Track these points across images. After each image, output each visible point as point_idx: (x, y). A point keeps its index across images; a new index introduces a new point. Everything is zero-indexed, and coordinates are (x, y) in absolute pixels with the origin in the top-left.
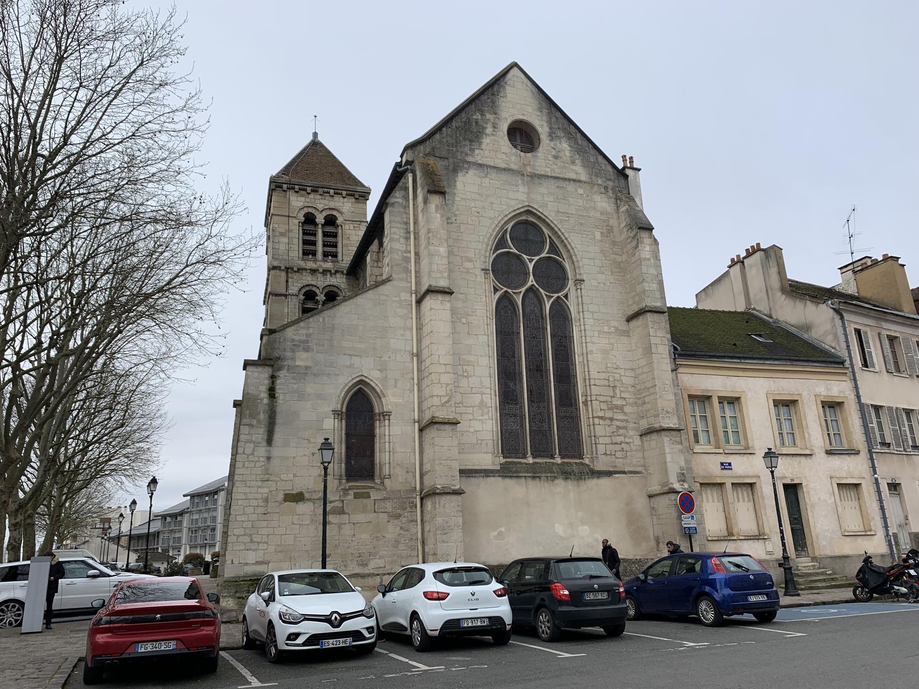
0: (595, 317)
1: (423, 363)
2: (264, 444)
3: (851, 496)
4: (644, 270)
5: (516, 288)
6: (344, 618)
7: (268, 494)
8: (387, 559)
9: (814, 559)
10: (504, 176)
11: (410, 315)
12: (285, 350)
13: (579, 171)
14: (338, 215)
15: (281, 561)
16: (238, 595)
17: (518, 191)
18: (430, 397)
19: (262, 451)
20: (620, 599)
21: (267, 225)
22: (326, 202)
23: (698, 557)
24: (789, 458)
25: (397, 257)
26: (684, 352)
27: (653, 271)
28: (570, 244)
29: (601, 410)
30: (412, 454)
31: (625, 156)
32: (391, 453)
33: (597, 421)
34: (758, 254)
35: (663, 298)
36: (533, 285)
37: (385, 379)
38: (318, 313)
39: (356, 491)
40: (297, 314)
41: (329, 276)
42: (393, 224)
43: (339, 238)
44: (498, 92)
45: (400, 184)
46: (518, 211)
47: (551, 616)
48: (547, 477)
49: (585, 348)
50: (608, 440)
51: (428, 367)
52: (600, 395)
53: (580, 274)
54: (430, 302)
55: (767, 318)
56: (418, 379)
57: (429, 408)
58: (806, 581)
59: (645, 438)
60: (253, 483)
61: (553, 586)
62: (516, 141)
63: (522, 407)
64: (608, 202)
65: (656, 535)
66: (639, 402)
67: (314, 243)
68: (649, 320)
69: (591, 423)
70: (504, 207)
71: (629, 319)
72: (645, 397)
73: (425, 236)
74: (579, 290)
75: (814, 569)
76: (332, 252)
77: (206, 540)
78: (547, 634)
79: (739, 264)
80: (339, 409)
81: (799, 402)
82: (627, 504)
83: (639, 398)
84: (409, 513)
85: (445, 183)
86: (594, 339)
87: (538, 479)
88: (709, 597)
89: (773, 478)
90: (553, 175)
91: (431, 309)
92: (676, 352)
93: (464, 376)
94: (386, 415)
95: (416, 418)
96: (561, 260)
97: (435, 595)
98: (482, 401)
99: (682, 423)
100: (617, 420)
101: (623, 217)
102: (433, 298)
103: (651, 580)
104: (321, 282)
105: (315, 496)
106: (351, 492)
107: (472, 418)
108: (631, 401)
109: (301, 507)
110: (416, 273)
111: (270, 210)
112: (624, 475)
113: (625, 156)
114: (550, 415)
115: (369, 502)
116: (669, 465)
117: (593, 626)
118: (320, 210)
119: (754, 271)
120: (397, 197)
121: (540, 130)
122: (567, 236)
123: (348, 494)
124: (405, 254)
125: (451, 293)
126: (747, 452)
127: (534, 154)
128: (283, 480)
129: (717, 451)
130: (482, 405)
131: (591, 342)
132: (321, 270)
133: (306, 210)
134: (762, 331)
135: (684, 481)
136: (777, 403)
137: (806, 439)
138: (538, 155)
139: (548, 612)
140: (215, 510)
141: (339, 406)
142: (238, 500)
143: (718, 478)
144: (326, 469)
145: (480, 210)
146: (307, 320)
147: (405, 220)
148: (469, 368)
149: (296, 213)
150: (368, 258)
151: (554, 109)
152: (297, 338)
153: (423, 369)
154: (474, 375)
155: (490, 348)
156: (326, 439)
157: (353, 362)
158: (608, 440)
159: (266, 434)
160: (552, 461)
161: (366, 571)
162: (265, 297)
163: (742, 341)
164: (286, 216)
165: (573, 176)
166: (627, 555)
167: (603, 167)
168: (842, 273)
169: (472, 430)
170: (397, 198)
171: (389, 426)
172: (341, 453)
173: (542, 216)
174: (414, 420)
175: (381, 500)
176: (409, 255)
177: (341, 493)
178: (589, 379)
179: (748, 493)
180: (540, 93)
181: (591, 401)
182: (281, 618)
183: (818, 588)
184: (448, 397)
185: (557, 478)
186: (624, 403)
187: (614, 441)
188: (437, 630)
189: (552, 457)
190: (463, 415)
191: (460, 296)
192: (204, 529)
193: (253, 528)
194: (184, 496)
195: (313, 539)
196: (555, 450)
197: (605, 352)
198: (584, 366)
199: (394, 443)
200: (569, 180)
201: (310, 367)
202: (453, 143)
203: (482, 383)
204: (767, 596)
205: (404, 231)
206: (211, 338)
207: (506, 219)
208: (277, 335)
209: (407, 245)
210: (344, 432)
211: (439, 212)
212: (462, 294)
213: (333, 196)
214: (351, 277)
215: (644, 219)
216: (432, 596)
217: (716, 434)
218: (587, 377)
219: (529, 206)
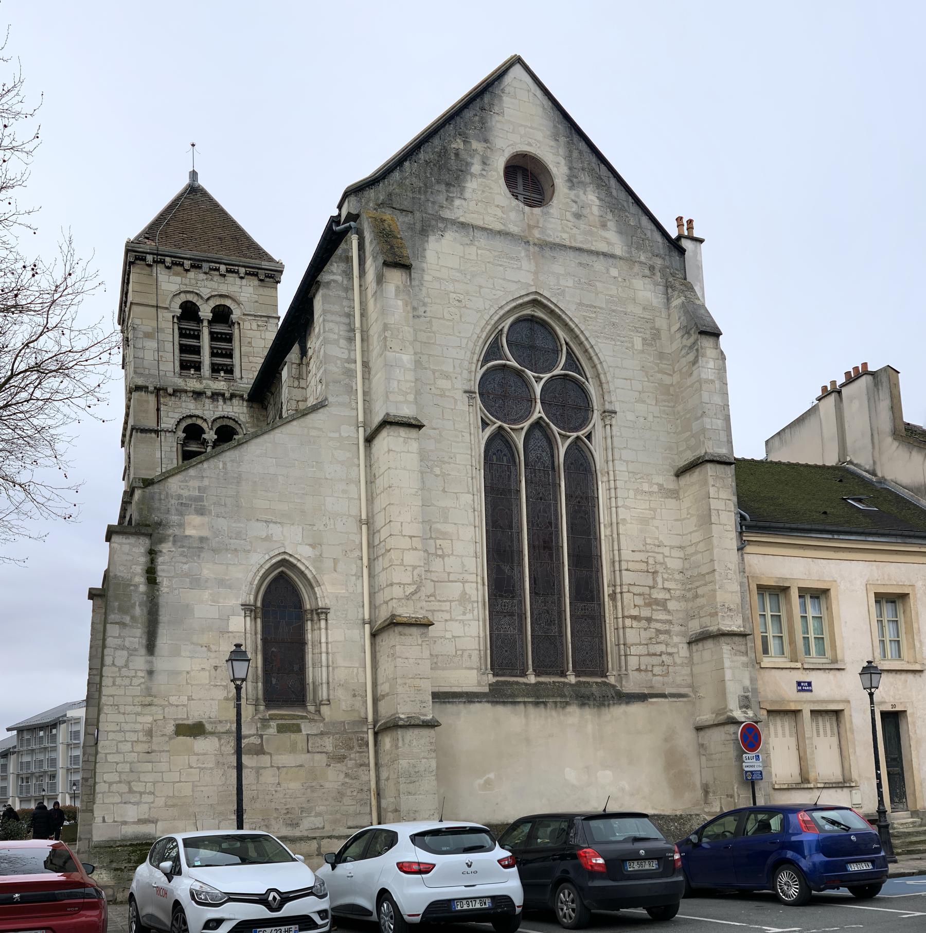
1: (377, 535)
2: (143, 651)
4: (705, 396)
5: (515, 422)
6: (286, 898)
7: (151, 724)
8: (327, 817)
9: (915, 813)
10: (499, 244)
11: (356, 460)
16: (114, 865)
17: (520, 268)
18: (387, 586)
19: (140, 662)
20: (674, 869)
21: (122, 320)
22: (214, 285)
23: (772, 811)
25: (335, 369)
26: (754, 523)
27: (717, 399)
28: (597, 355)
29: (635, 606)
30: (361, 670)
31: (681, 218)
32: (331, 668)
33: (628, 622)
34: (864, 380)
35: (730, 442)
36: (541, 418)
37: (319, 558)
38: (207, 459)
39: (280, 722)
40: (175, 461)
41: (221, 402)
42: (329, 317)
43: (236, 343)
44: (491, 105)
45: (339, 251)
46: (520, 301)
47: (578, 893)
48: (555, 703)
49: (614, 516)
50: (642, 650)
51: (384, 541)
52: (634, 585)
53: (611, 402)
54: (387, 440)
55: (868, 476)
56: (369, 559)
57: (386, 603)
58: (903, 842)
59: (694, 647)
60: (129, 709)
61: (581, 852)
62: (516, 188)
63: (522, 602)
64: (654, 292)
65: (704, 782)
66: (689, 595)
67: (197, 351)
68: (709, 474)
69: (621, 625)
71: (681, 472)
72: (697, 587)
73: (379, 336)
74: (608, 427)
75: (914, 826)
76: (225, 365)
77: (44, 790)
78: (571, 918)
79: (833, 394)
80: (252, 602)
81: (911, 596)
82: (666, 740)
83: (690, 590)
84: (357, 754)
85: (408, 252)
86: (629, 502)
87: (542, 706)
88: (792, 865)
89: (872, 702)
90: (574, 244)
91: (389, 451)
92: (744, 522)
93: (437, 555)
94: (321, 613)
95: (367, 617)
96: (583, 380)
97: (415, 867)
98: (464, 593)
99: (747, 626)
100: (657, 621)
101: (675, 315)
102: (392, 433)
103: (707, 843)
104: (210, 411)
105: (221, 728)
106: (273, 724)
107: (448, 618)
108: (678, 593)
109: (202, 744)
111: (126, 297)
112: (663, 700)
113: (681, 218)
114: (561, 614)
115: (299, 738)
117: (636, 907)
118: (206, 297)
119: (856, 405)
120: (333, 273)
121: (554, 169)
122: (593, 343)
123: (269, 727)
124: (346, 365)
125: (420, 427)
126: (835, 668)
128: (172, 705)
129: (793, 665)
130: (464, 598)
131: (624, 506)
132: (209, 393)
133: (183, 298)
134: (862, 494)
135: (747, 707)
136: (880, 598)
137: (917, 649)
138: (551, 211)
139: (573, 889)
140: (54, 749)
141: (252, 598)
142: (108, 732)
144: (238, 688)
145: (462, 297)
146: (200, 466)
147: (347, 310)
148: (445, 544)
149: (168, 302)
150: (285, 373)
151: (576, 138)
152: (185, 493)
153: (376, 544)
154: (452, 554)
155: (476, 513)
156: (238, 646)
157: (270, 532)
158: (642, 650)
160: (562, 680)
161: (297, 833)
162: (124, 435)
163: (834, 508)
164: (153, 306)
165: (602, 247)
166: (663, 810)
167: (649, 234)
169: (448, 635)
170: (334, 274)
171: (327, 629)
172: (257, 667)
173: (557, 310)
174: (364, 620)
176: (352, 366)
177: (259, 725)
178: (620, 561)
179: (831, 725)
180: (555, 109)
181: (621, 593)
182: (193, 898)
183: (919, 852)
184: (415, 587)
186: (668, 596)
187: (652, 651)
188: (419, 915)
189: (563, 674)
190: (435, 613)
191: (431, 432)
192: (40, 776)
193: (132, 772)
194: (9, 730)
195: (221, 789)
196: (568, 664)
197: (644, 521)
198: (613, 541)
199: (334, 654)
200: (598, 253)
202: (420, 188)
203: (463, 566)
204: (873, 865)
205: (343, 328)
206: (54, 491)
207: (502, 312)
208: (155, 488)
209: (349, 351)
210: (259, 636)
211: (401, 298)
212: (434, 429)
213: (224, 276)
214: (255, 406)
215: (708, 319)
216: (410, 867)
217: (792, 642)
218: (617, 558)
219: (536, 293)
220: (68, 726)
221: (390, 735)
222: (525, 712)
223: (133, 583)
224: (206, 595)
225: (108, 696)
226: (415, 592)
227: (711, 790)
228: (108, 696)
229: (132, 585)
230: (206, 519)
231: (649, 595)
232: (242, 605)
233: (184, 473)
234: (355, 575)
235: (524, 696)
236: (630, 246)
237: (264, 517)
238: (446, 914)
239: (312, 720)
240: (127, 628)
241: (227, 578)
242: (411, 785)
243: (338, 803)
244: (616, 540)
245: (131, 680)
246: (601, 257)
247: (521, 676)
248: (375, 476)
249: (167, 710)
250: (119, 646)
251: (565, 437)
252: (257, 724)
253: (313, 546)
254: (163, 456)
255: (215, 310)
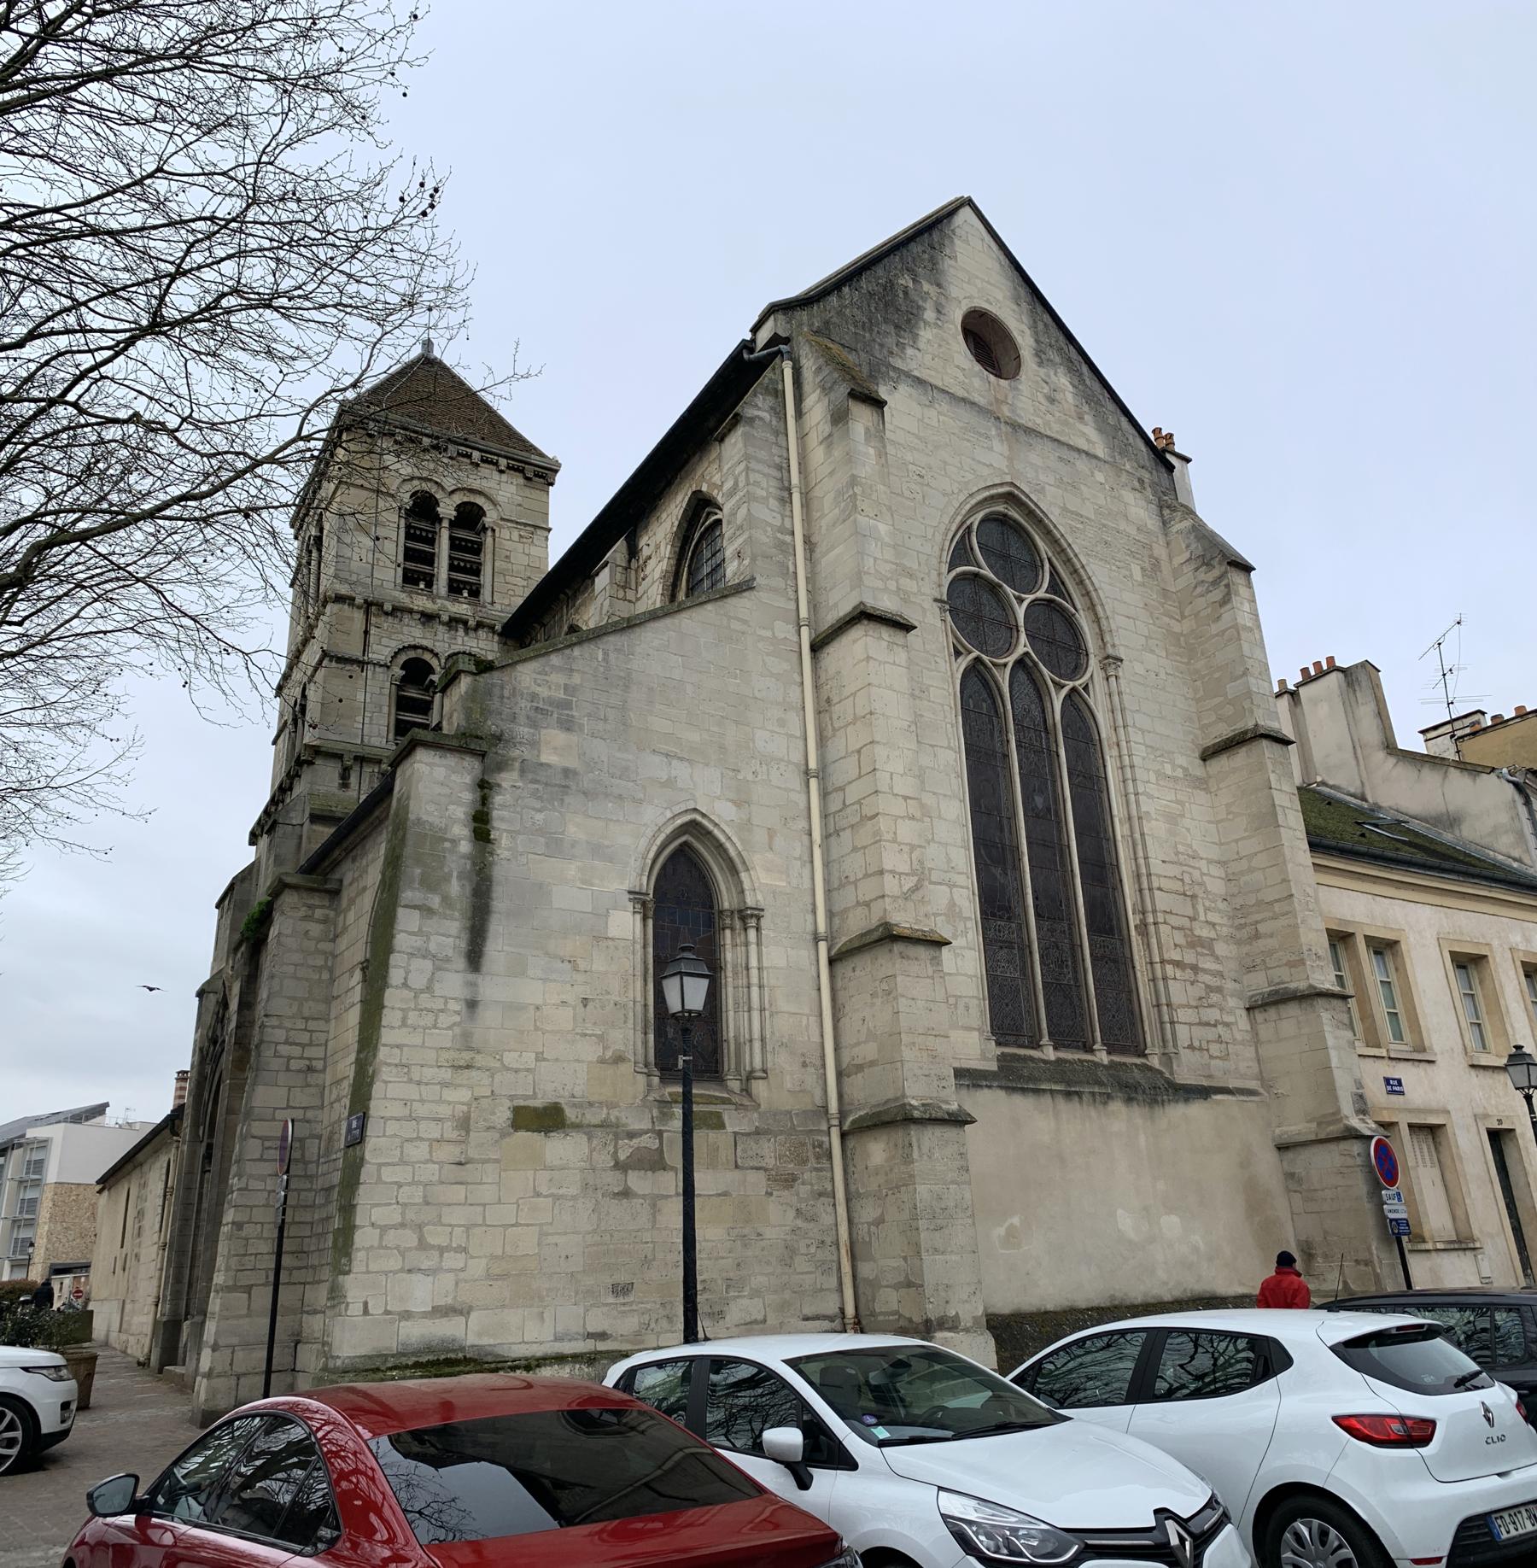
0: (1148, 743)
2: (460, 963)
3: (1422, 1156)
7: (469, 1105)
10: (964, 413)
12: (514, 718)
13: (1088, 435)
14: (486, 506)
15: (503, 1306)
17: (991, 449)
19: (454, 983)
24: (1489, 1073)
25: (764, 538)
28: (1089, 578)
29: (1176, 945)
30: (813, 1020)
34: (1334, 677)
41: (461, 632)
46: (993, 491)
48: (1093, 1094)
52: (1171, 913)
53: (1114, 646)
59: (1259, 1016)
60: (429, 1073)
66: (1244, 934)
67: (429, 559)
68: (1267, 755)
70: (970, 476)
71: (1209, 754)
98: (952, 904)
100: (1205, 971)
102: (871, 633)
104: (443, 642)
108: (1225, 931)
109: (562, 1149)
110: (807, 583)
112: (1230, 1097)
116: (1337, 1074)
118: (450, 489)
119: (1323, 709)
121: (1019, 339)
124: (779, 535)
125: (907, 628)
126: (1421, 1057)
127: (1013, 383)
128: (508, 1069)
132: (445, 618)
143: (1385, 1112)
146: (567, 652)
147: (777, 460)
151: (1040, 309)
152: (543, 692)
157: (674, 773)
159: (465, 936)
165: (1081, 443)
168: (1426, 741)
170: (759, 409)
171: (759, 944)
175: (748, 1134)
177: (655, 1112)
184: (916, 878)
185: (1112, 1098)
186: (1213, 935)
187: (1205, 1019)
189: (1091, 1051)
193: (428, 1204)
196: (1093, 1032)
199: (772, 988)
200: (1079, 451)
201: (575, 773)
203: (949, 861)
208: (494, 678)
209: (783, 517)
214: (509, 643)
220: (25, 1152)
221: (885, 1137)
222: (1054, 1108)
223: (448, 836)
224: (572, 869)
225: (392, 1046)
226: (916, 888)
227: (1319, 1252)
228: (392, 1046)
229: (447, 840)
230: (574, 738)
231: (1191, 930)
232: (630, 892)
233: (542, 660)
234: (800, 859)
235: (1049, 1080)
236: (1113, 449)
237: (664, 748)
238: (1490, 1555)
239: (739, 1107)
240: (435, 918)
241: (606, 843)
242: (937, 1234)
243: (787, 1269)
244: (1139, 842)
245: (437, 1017)
246: (1084, 456)
247: (1033, 1048)
248: (828, 700)
249: (498, 1077)
250: (419, 950)
251: (1060, 687)
252: (651, 1112)
253: (738, 804)
254: (368, 700)
255: (460, 508)
